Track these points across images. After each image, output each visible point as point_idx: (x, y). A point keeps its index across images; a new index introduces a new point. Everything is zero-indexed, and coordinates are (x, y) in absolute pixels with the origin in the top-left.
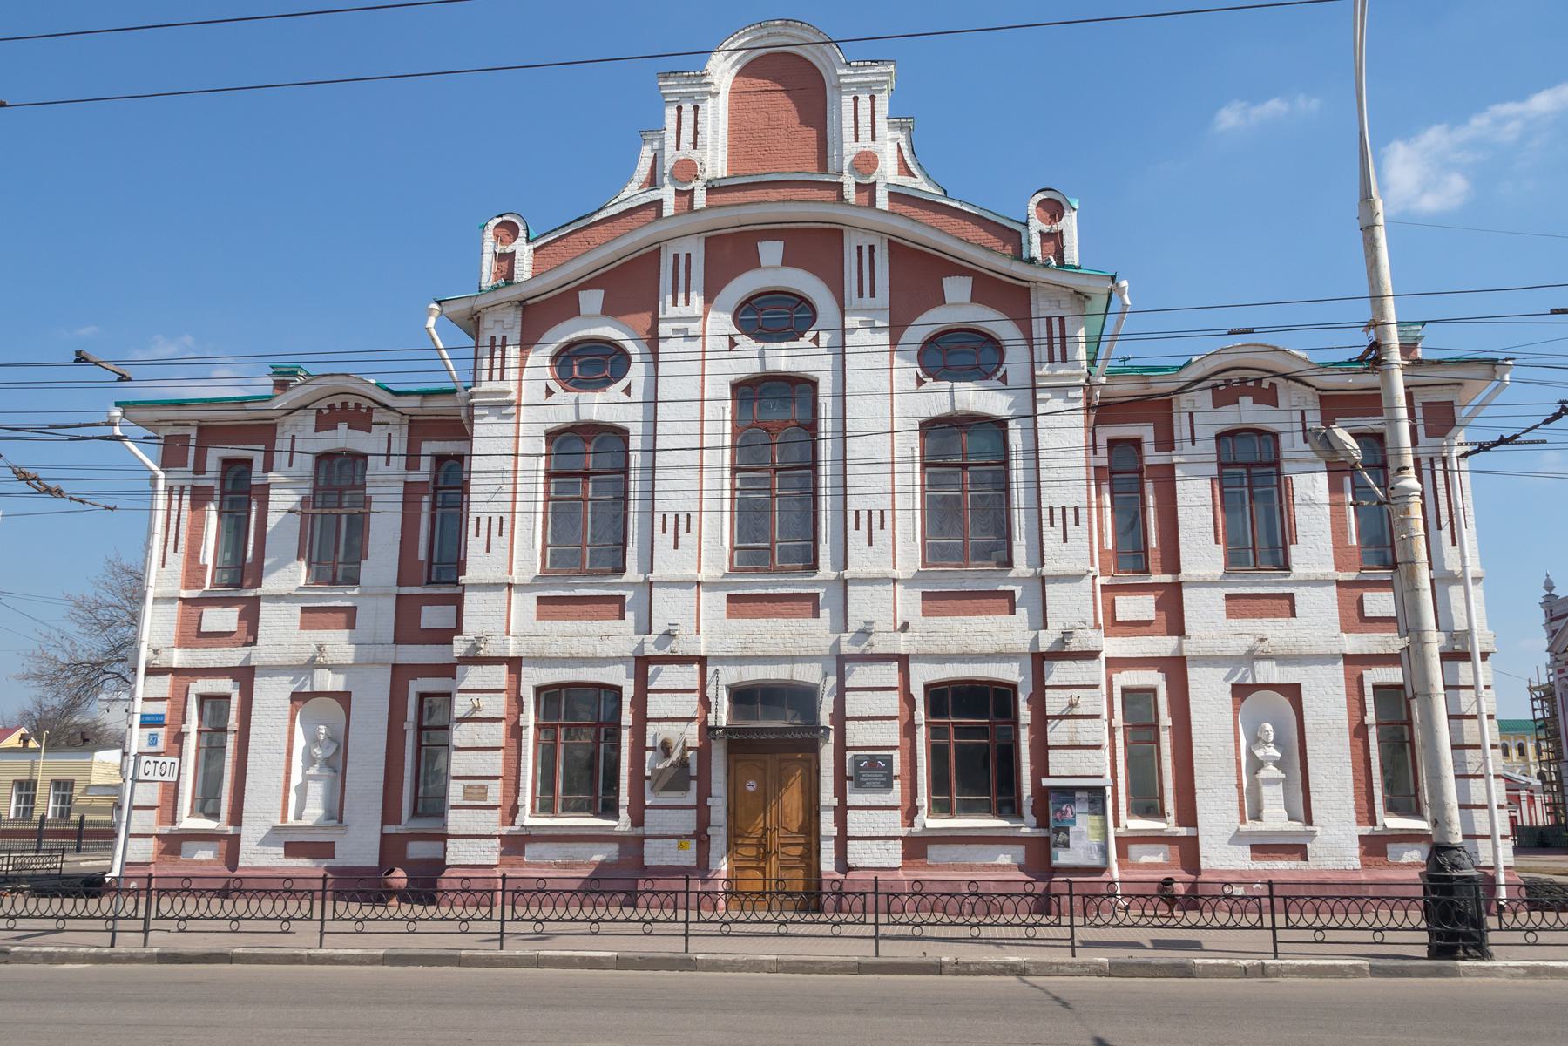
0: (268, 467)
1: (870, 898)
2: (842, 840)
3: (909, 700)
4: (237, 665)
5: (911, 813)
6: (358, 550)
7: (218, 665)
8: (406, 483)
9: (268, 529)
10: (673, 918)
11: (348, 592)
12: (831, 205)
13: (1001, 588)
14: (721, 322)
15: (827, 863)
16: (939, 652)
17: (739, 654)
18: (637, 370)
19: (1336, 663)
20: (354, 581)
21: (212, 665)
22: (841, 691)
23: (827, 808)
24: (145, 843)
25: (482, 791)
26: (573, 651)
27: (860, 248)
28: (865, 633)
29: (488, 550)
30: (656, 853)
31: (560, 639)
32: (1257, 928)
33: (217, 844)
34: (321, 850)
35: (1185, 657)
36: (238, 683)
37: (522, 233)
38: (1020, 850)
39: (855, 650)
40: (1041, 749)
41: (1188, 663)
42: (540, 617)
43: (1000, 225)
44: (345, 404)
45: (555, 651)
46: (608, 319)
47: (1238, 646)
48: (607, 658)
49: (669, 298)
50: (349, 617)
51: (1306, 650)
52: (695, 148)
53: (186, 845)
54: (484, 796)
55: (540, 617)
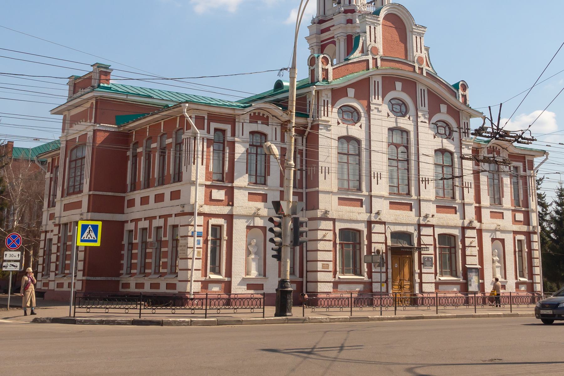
0: (233, 135)
1: (205, 301)
2: (421, 283)
3: (335, 234)
4: (226, 213)
5: (436, 274)
6: (267, 171)
7: (219, 213)
8: (281, 147)
9: (236, 160)
10: (136, 308)
11: (265, 188)
12: (412, 73)
13: (454, 206)
14: (385, 108)
15: (417, 291)
16: (441, 225)
17: (394, 222)
18: (363, 120)
19: (511, 233)
20: (265, 184)
21: (217, 213)
22: (419, 235)
23: (417, 273)
24: (197, 284)
25: (327, 266)
26: (351, 218)
27: (421, 90)
28: (378, 213)
29: (325, 179)
30: (376, 288)
31: (347, 213)
32: (135, 309)
33: (220, 285)
34: (259, 287)
35: (233, 215)
36: (226, 221)
37: (330, 62)
38: (459, 286)
39: (424, 223)
40: (464, 256)
41: (483, 231)
42: (339, 205)
43: (451, 89)
44: (259, 113)
45: (346, 217)
46: (355, 100)
47: (493, 227)
48: (360, 221)
49: (373, 97)
50: (264, 198)
51: (507, 229)
52: (375, 43)
53: (210, 285)
54: (328, 268)
55: (339, 205)
